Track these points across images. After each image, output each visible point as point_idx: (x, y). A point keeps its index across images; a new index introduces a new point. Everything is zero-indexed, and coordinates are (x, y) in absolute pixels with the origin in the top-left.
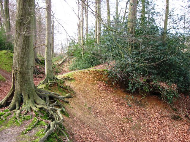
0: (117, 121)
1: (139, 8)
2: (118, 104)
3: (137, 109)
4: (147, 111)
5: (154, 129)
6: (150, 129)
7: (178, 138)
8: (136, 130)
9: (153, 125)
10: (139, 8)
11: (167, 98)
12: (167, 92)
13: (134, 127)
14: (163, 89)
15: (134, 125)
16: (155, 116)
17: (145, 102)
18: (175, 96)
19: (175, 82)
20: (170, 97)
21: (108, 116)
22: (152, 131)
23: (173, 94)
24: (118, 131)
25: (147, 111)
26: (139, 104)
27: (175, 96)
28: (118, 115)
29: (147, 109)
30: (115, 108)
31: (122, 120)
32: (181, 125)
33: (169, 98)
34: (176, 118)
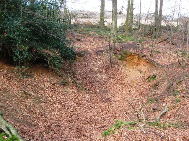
0: (16, 98)
1: (107, 20)
2: (7, 79)
3: (27, 81)
4: (37, 82)
5: (52, 98)
6: (49, 99)
7: (75, 102)
8: (38, 104)
9: (49, 94)
10: (107, 20)
11: (54, 64)
12: (53, 58)
13: (36, 101)
14: (49, 56)
15: (34, 98)
16: (47, 85)
17: (31, 73)
18: (60, 62)
19: (56, 48)
20: (57, 63)
21: (4, 95)
22: (52, 101)
23: (59, 60)
24: (26, 109)
25: (37, 82)
26: (26, 76)
27: (60, 62)
28: (15, 91)
29: (35, 79)
30: (6, 84)
31: (22, 96)
32: (70, 90)
33: (56, 64)
34: (64, 84)
